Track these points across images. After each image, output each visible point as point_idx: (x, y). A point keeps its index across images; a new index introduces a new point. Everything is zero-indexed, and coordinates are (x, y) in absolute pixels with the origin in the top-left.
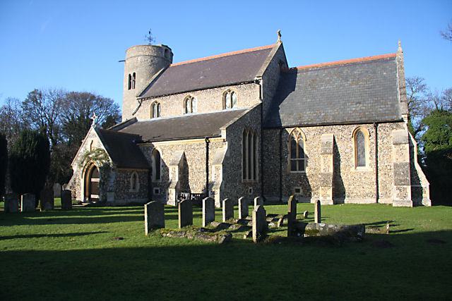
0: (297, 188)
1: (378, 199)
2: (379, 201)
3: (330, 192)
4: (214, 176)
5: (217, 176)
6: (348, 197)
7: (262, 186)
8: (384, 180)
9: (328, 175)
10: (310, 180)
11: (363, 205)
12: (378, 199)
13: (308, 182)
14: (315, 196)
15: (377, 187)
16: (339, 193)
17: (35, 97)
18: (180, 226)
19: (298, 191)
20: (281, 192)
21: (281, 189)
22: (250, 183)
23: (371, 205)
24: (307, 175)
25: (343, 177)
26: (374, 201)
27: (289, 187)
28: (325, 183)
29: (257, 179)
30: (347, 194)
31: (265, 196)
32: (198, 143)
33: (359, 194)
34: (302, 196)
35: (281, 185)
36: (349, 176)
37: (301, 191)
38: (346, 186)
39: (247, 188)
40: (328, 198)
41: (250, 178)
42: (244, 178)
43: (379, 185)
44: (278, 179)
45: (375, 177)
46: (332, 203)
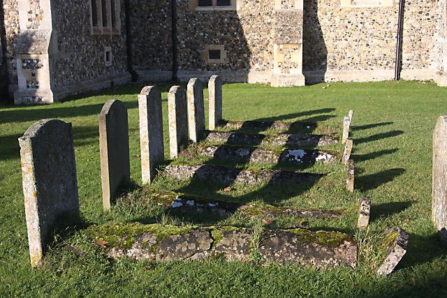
0: (212, 47)
1: (399, 69)
2: (403, 75)
3: (298, 57)
4: (27, 16)
5: (36, 18)
6: (333, 67)
7: (128, 43)
8: (417, 26)
9: (292, 16)
10: (245, 27)
11: (364, 85)
12: (399, 69)
13: (241, 34)
14: (257, 65)
15: (401, 42)
16: (315, 60)
17: (352, 81)
18: (35, 245)
19: (215, 54)
20: (175, 58)
21: (174, 50)
22: (107, 37)
23: (383, 84)
24: (240, 15)
25: (324, 21)
26: (390, 74)
27: (193, 46)
28: (284, 36)
29: (119, 25)
30: (329, 60)
31: (134, 67)
32: (295, 47)
33: (357, 60)
34: (224, 67)
35: (175, 41)
36: (337, 19)
37: (223, 55)
38: (328, 43)
39: (102, 49)
40: (293, 71)
41: (105, 24)
42: (95, 23)
43: (405, 39)
44: (167, 25)
45: (394, 20)
46: (302, 82)
